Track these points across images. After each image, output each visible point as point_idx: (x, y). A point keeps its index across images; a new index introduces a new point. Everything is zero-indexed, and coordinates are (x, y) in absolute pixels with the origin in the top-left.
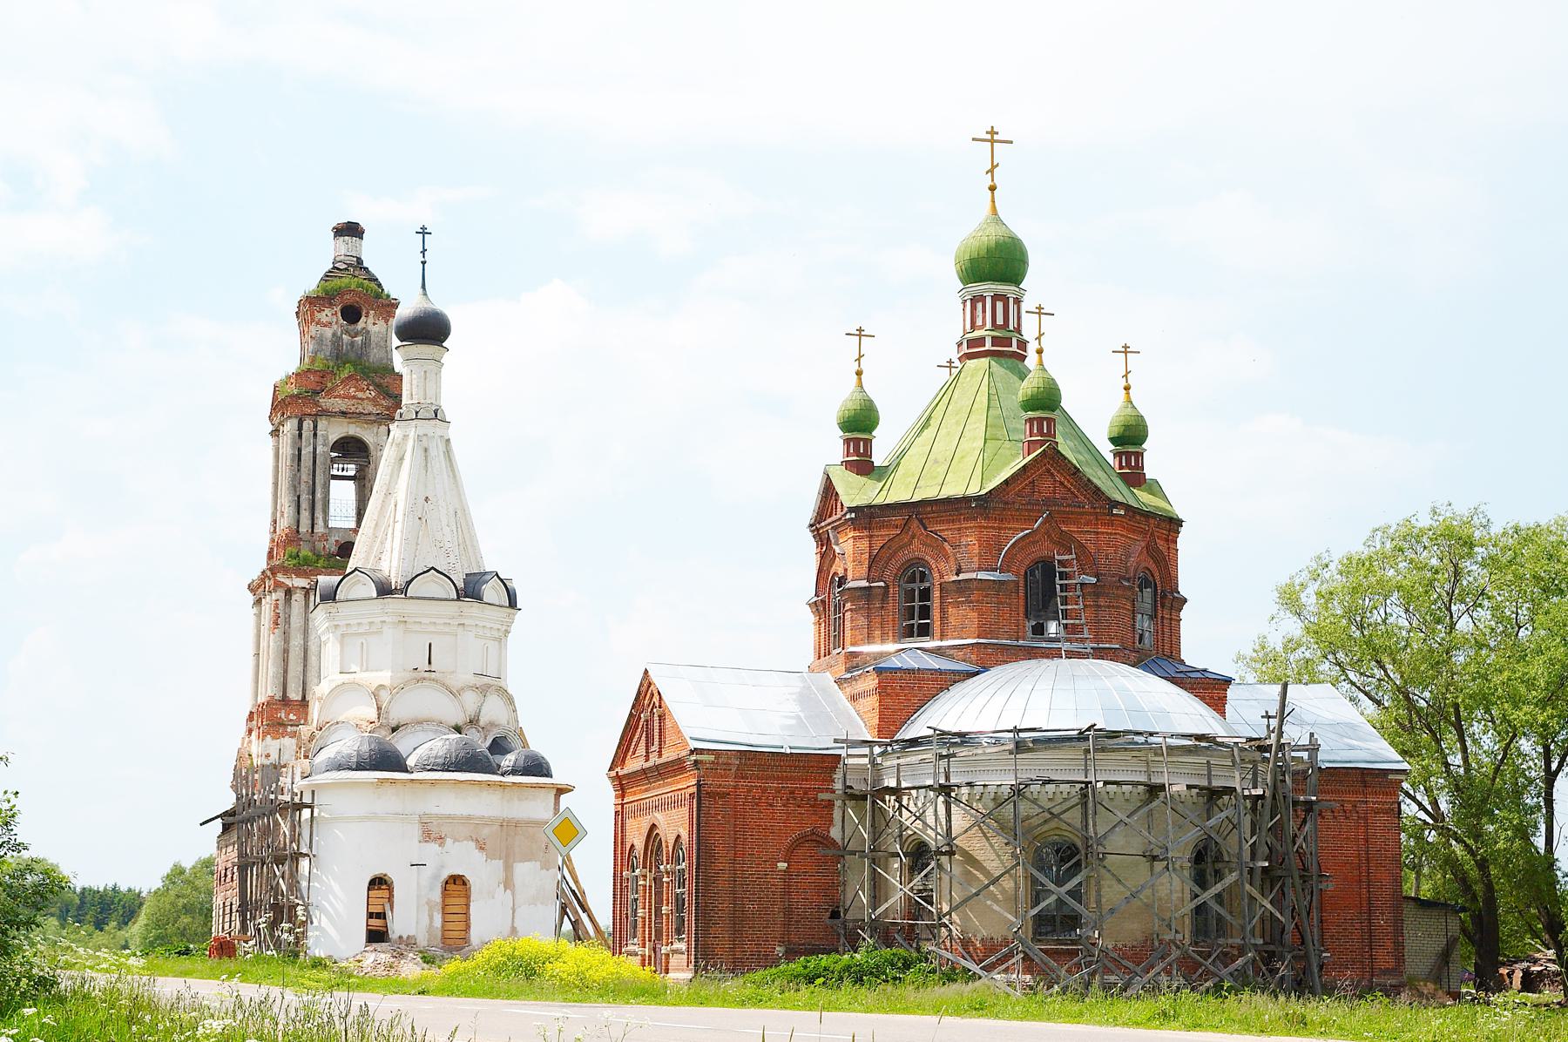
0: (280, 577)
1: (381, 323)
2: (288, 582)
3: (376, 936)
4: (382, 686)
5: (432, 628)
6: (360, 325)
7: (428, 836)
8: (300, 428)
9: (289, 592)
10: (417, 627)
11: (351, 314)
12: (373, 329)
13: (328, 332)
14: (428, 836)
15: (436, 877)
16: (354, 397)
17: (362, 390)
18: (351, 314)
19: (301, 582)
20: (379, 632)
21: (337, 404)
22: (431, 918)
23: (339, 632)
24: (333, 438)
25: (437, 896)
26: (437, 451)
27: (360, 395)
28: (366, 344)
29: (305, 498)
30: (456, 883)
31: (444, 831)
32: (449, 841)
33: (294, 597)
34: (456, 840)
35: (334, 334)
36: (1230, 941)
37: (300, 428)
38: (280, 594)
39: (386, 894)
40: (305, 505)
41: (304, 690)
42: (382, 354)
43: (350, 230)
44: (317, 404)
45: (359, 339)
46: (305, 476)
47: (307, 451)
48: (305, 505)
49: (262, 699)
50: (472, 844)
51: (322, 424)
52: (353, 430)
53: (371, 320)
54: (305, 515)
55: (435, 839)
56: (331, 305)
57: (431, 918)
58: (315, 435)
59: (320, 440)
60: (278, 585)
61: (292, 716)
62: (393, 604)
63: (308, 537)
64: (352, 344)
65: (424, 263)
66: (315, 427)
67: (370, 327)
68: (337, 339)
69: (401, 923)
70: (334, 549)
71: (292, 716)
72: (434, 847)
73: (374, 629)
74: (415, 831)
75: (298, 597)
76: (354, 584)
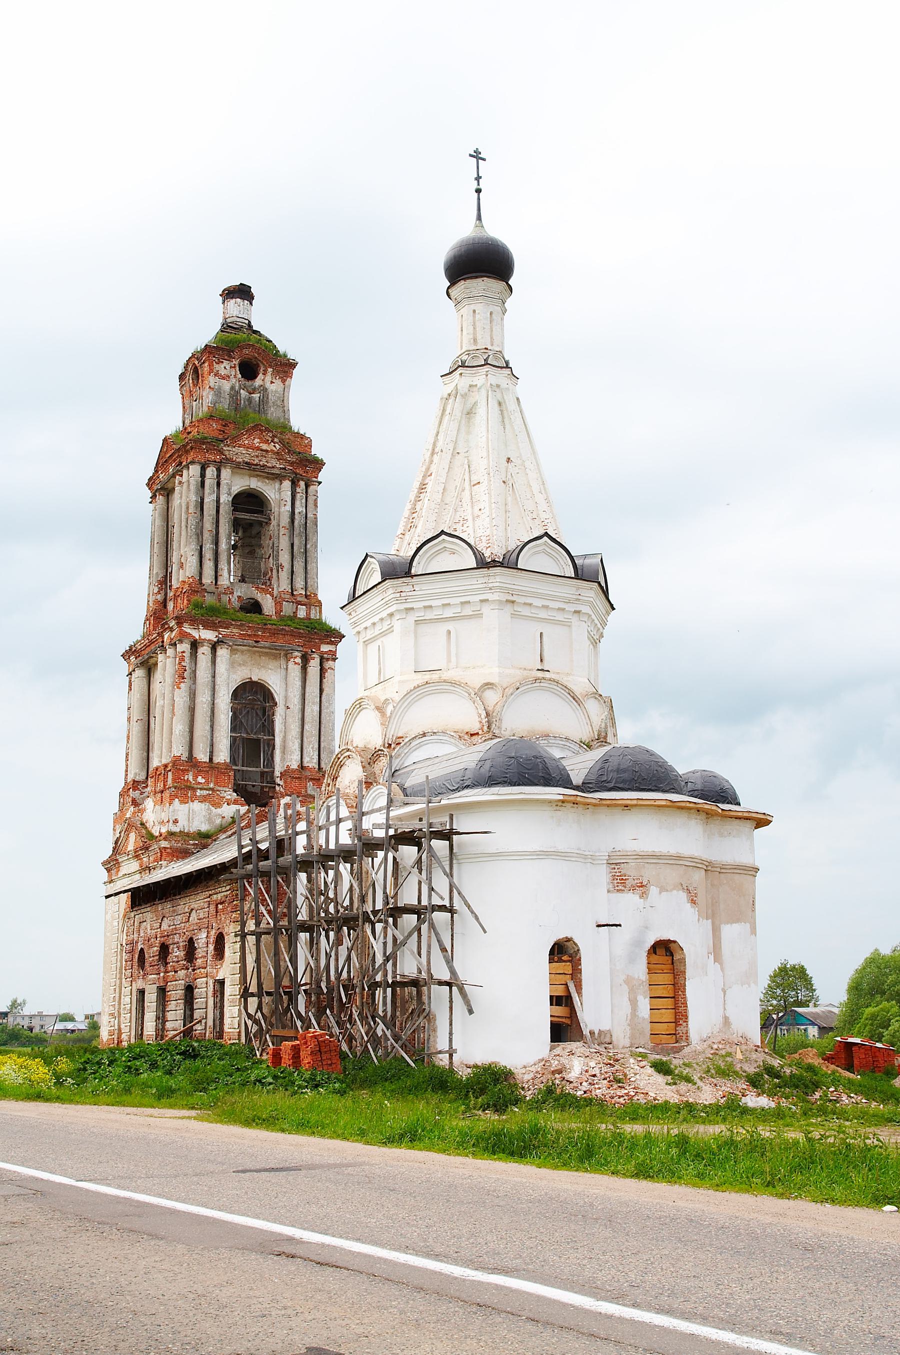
0: (187, 628)
1: (278, 382)
2: (195, 634)
3: (562, 1031)
4: (489, 685)
5: (543, 614)
6: (258, 382)
7: (620, 882)
8: (203, 475)
9: (195, 645)
10: (526, 611)
11: (249, 371)
12: (272, 388)
13: (226, 386)
14: (620, 882)
15: (637, 943)
16: (258, 449)
17: (267, 442)
18: (249, 371)
19: (209, 635)
20: (478, 616)
21: (239, 453)
22: (634, 1003)
23: (412, 618)
24: (236, 490)
25: (640, 970)
26: (511, 405)
27: (264, 446)
28: (264, 401)
29: (208, 547)
30: (664, 950)
31: (648, 873)
32: (653, 890)
33: (201, 650)
34: (662, 889)
35: (232, 388)
36: (291, 1043)
37: (203, 475)
38: (185, 647)
39: (567, 968)
40: (208, 555)
41: (211, 753)
42: (279, 413)
43: (242, 292)
44: (221, 452)
45: (256, 396)
46: (208, 525)
47: (210, 499)
48: (208, 555)
49: (130, 778)
50: (683, 896)
51: (226, 473)
52: (254, 484)
53: (268, 378)
54: (209, 565)
55: (633, 888)
56: (230, 358)
57: (634, 1003)
58: (218, 484)
59: (224, 489)
60: (183, 636)
61: (200, 779)
62: (499, 576)
63: (212, 588)
64: (250, 400)
65: (478, 191)
66: (219, 476)
67: (268, 385)
68: (234, 394)
69: (593, 1012)
70: (236, 604)
71: (200, 779)
72: (631, 899)
73: (468, 611)
74: (603, 875)
75: (204, 651)
76: (438, 552)
